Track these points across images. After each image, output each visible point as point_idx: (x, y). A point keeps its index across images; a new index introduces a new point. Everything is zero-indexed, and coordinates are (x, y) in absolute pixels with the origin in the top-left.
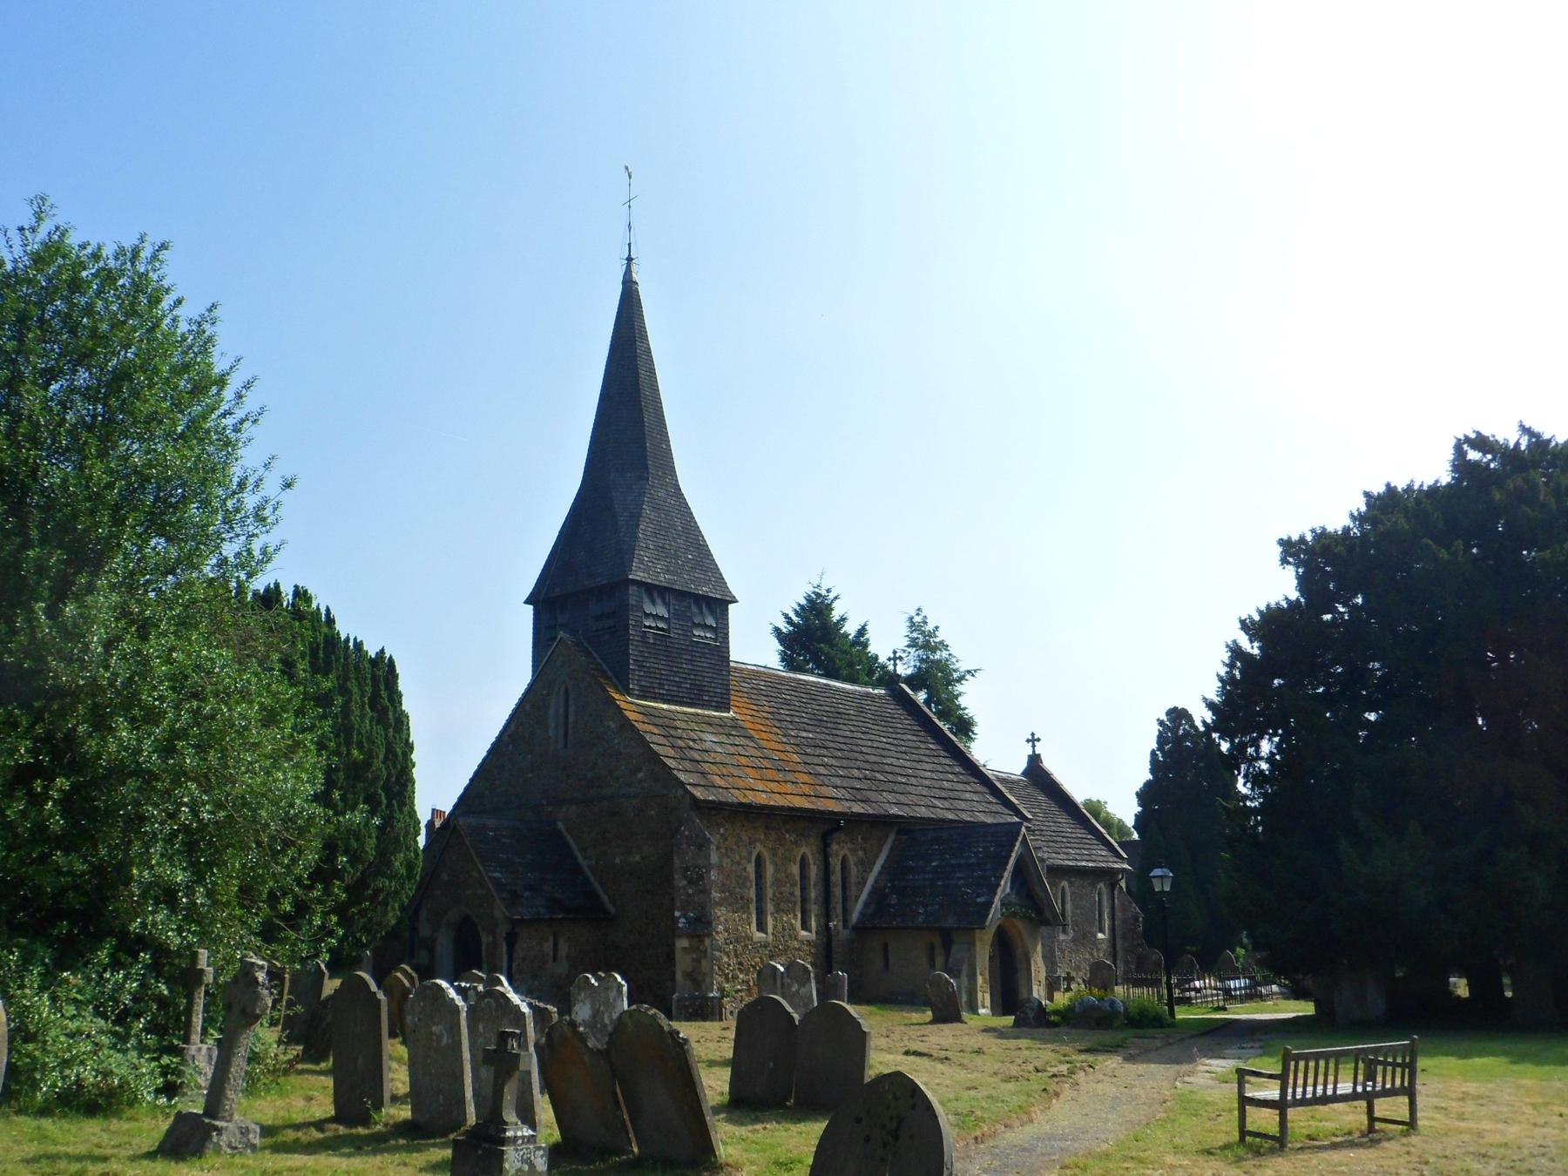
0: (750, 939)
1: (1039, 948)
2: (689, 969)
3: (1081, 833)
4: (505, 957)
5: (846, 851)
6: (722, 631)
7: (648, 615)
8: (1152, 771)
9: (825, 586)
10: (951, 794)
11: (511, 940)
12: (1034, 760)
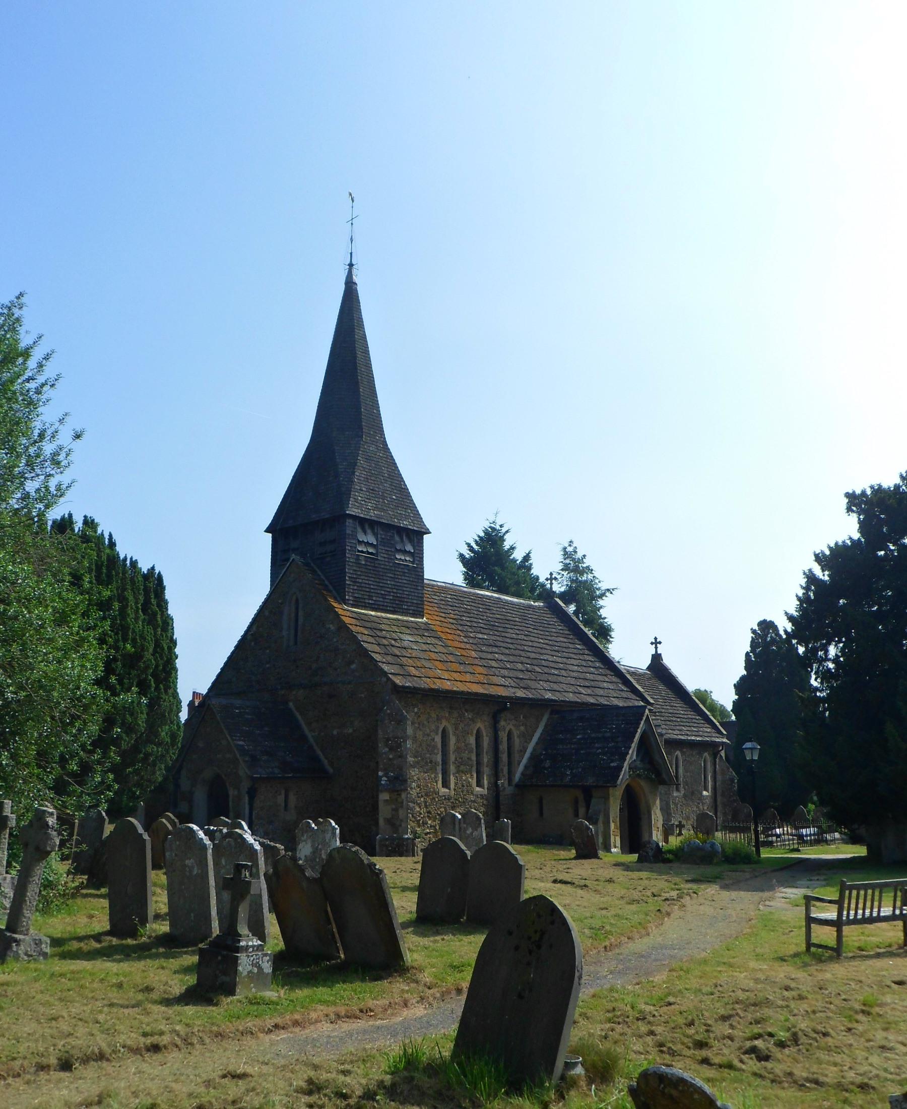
1: (658, 802)
2: (389, 816)
3: (691, 714)
4: (247, 807)
6: (418, 556)
7: (360, 542)
8: (746, 668)
9: (499, 523)
11: (252, 793)
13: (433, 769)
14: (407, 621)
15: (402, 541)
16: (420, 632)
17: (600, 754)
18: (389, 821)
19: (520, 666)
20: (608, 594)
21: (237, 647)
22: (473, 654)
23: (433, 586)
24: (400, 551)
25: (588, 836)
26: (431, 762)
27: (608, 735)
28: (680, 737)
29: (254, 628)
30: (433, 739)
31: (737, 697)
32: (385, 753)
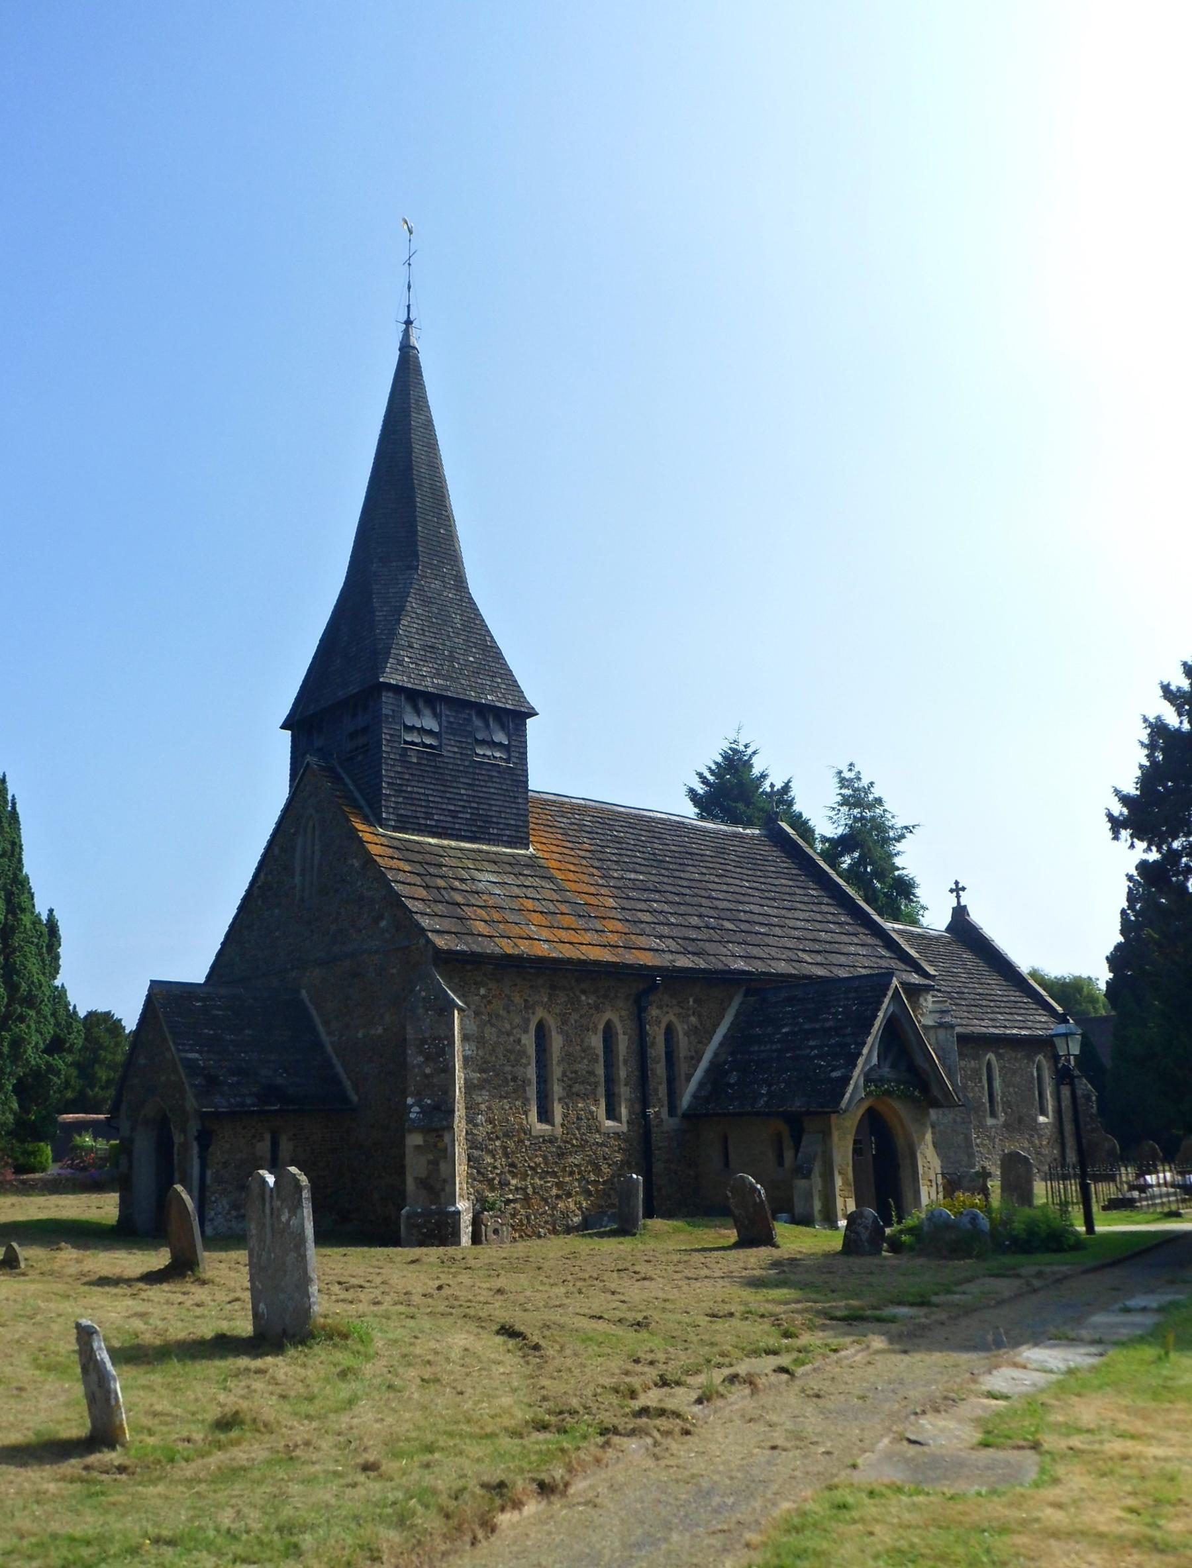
0: (528, 1132)
1: (929, 1137)
2: (423, 1174)
3: (1015, 995)
4: (196, 1162)
6: (517, 749)
8: (1122, 932)
9: (742, 742)
11: (205, 1139)
12: (960, 912)
14: (488, 853)
15: (487, 726)
16: (517, 870)
17: (816, 1057)
18: (423, 1183)
19: (695, 921)
20: (908, 835)
21: (241, 908)
22: (611, 902)
23: (563, 803)
24: (482, 742)
25: (755, 1203)
26: (514, 1079)
27: (831, 1024)
28: (992, 1030)
29: (262, 876)
30: (519, 1041)
31: (1111, 975)
32: (419, 1066)
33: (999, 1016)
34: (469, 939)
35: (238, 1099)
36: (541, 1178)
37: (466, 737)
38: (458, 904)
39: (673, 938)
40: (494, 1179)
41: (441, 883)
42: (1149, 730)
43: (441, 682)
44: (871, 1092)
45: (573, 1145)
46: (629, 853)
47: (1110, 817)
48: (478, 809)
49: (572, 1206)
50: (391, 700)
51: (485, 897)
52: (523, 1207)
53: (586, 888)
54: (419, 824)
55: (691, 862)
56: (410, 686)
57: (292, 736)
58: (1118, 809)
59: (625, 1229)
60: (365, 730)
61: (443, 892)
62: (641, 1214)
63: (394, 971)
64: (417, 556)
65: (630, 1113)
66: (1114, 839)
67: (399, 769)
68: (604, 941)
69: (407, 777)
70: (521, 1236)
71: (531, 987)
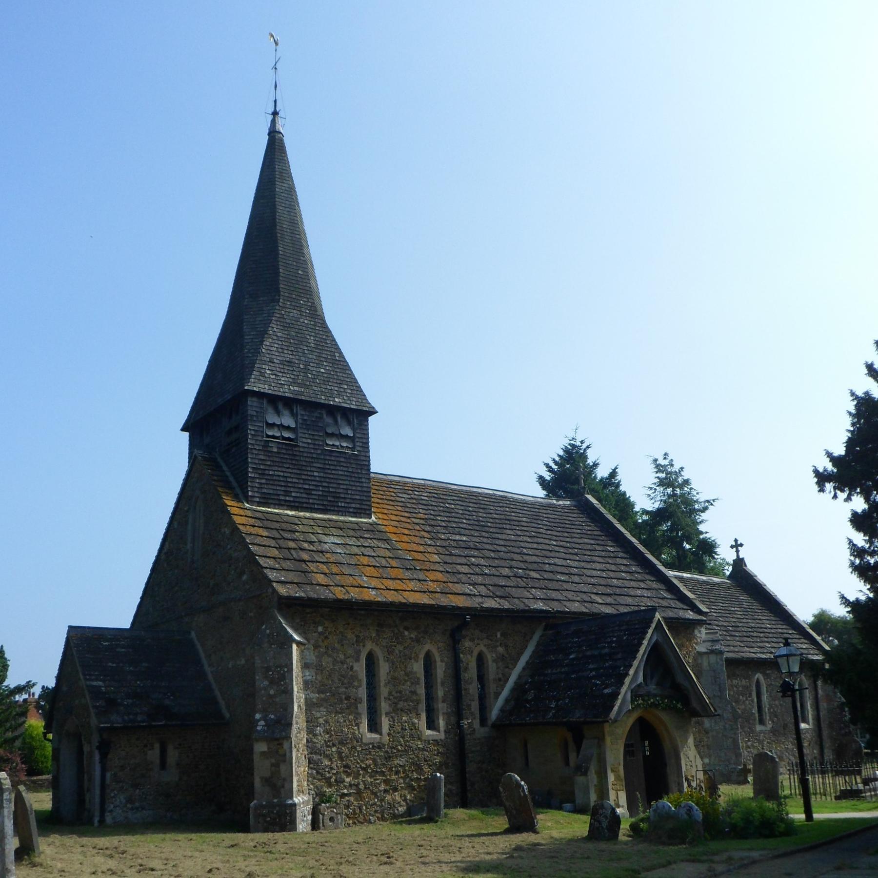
0: (359, 740)
1: (691, 741)
2: (267, 774)
5: (482, 648)
6: (361, 441)
7: (272, 426)
10: (618, 591)
11: (105, 748)
13: (352, 705)
14: (336, 521)
15: (336, 422)
16: (358, 534)
17: (594, 677)
18: (267, 781)
19: (506, 572)
21: (154, 570)
22: (436, 558)
23: (405, 483)
24: (332, 435)
26: (348, 698)
27: (606, 650)
30: (352, 668)
32: (265, 689)
33: (767, 645)
34: (308, 588)
35: (131, 717)
36: (371, 777)
37: (318, 431)
38: (304, 561)
39: (484, 585)
40: (331, 778)
41: (292, 544)
42: (855, 402)
43: (296, 389)
44: (639, 705)
45: (398, 750)
46: (456, 520)
47: (817, 473)
48: (328, 487)
49: (398, 798)
50: (255, 404)
51: (328, 555)
52: (356, 800)
53: (415, 547)
54: (279, 500)
55: (508, 527)
56: (270, 392)
57: (190, 437)
58: (826, 465)
59: (430, 819)
60: (237, 428)
61: (293, 552)
62: (442, 805)
63: (252, 614)
64: (279, 291)
65: (447, 724)
66: (820, 491)
67: (262, 457)
68: (424, 588)
69: (269, 463)
70: (354, 823)
71: (362, 625)
